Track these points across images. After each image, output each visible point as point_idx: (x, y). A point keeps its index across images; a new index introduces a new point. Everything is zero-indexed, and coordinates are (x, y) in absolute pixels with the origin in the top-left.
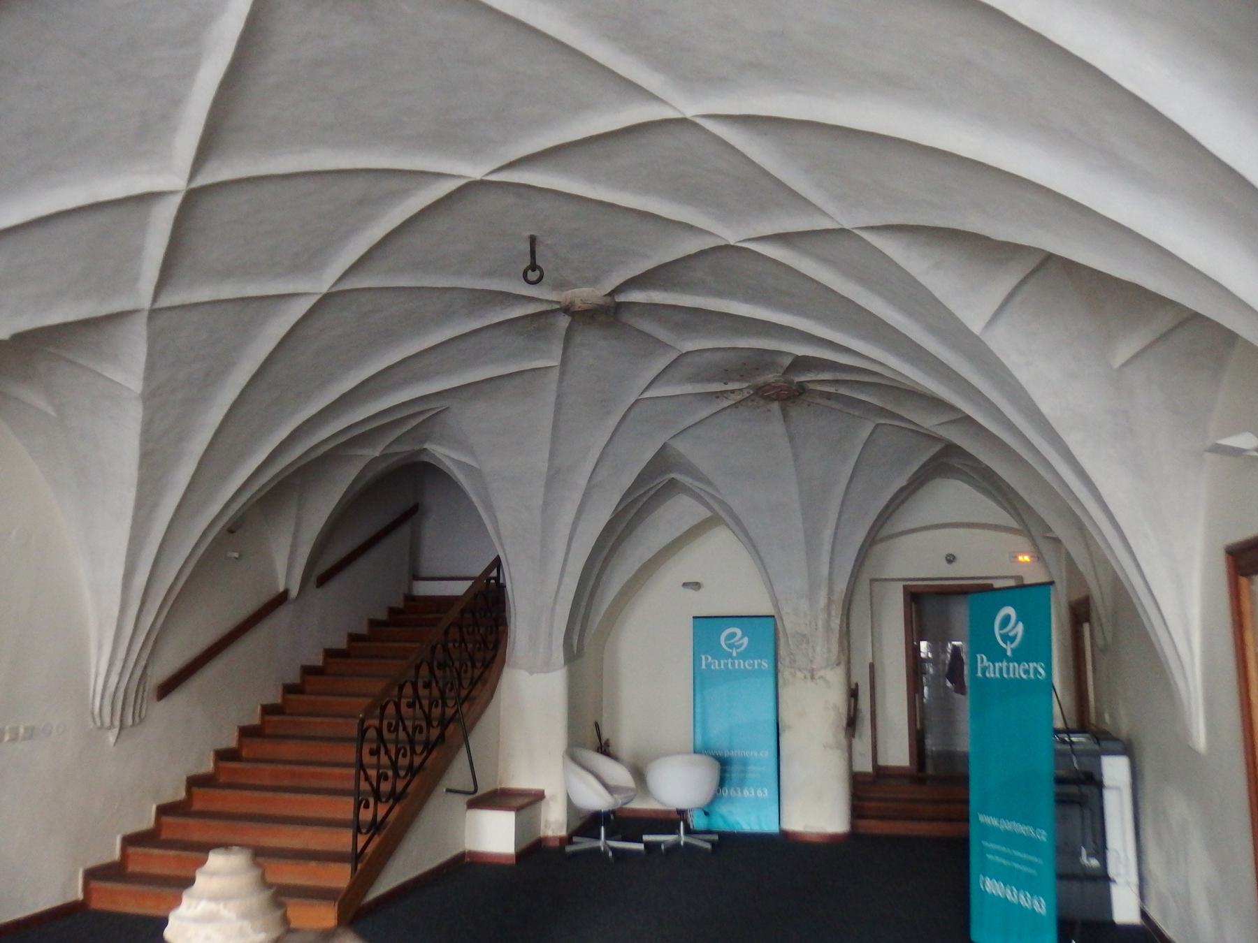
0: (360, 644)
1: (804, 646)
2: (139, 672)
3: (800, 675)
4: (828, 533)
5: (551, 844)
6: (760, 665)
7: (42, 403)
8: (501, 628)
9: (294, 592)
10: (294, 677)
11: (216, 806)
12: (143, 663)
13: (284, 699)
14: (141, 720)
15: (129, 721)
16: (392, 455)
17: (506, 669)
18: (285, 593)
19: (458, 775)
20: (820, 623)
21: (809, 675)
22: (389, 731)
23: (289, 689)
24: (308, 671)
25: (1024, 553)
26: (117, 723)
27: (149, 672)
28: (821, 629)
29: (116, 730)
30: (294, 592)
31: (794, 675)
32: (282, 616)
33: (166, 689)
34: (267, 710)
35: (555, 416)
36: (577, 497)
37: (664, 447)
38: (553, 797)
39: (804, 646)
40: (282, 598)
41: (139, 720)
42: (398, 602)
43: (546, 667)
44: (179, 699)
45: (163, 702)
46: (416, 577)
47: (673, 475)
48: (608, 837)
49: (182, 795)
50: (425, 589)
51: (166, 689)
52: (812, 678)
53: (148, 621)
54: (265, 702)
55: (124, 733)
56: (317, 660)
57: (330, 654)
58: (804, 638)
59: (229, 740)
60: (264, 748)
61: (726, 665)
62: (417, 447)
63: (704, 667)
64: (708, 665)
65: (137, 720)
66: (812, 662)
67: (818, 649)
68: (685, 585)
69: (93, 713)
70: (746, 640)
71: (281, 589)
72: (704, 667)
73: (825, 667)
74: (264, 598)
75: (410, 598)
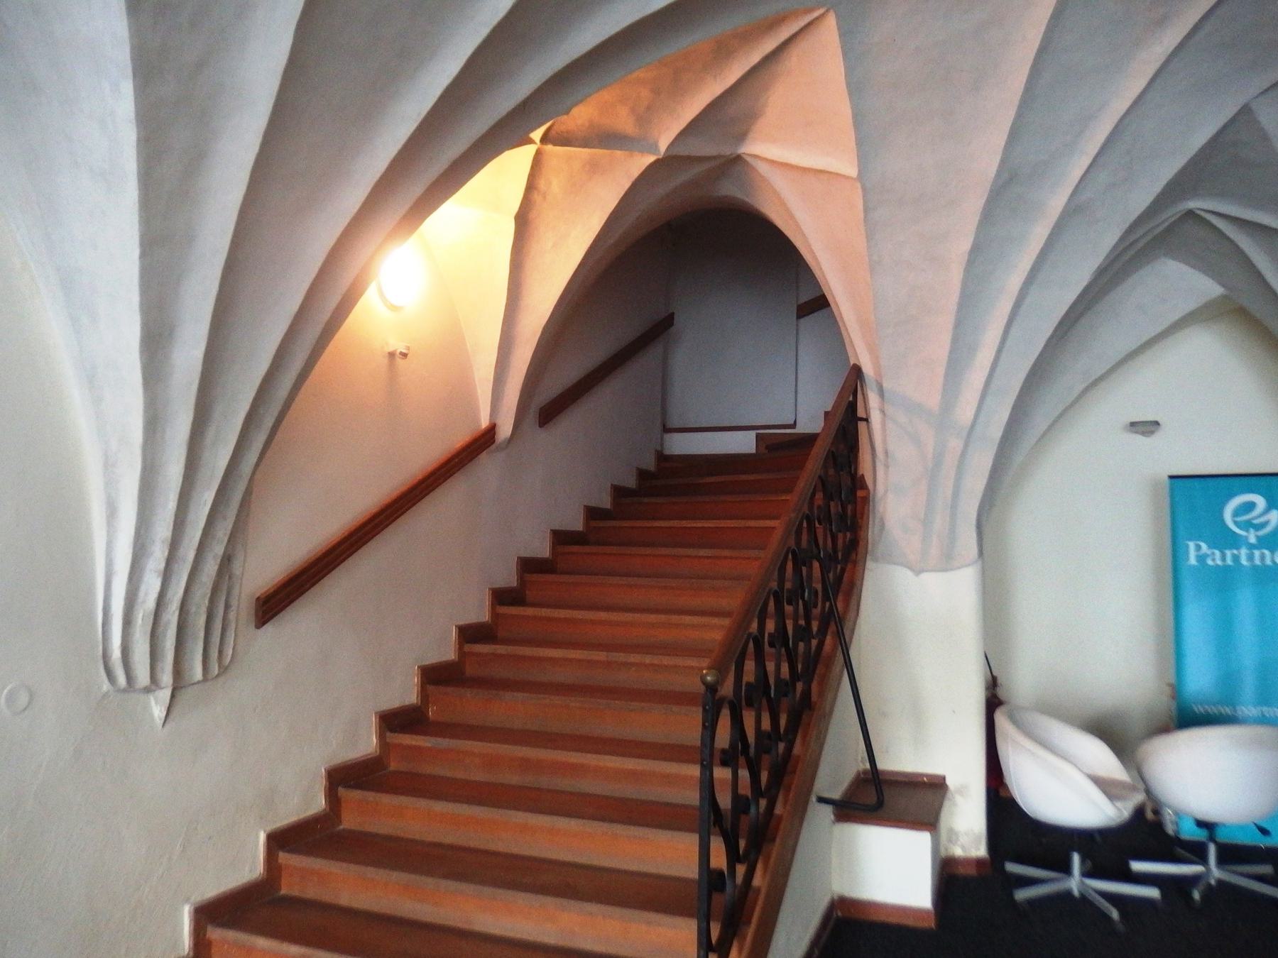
0: (601, 524)
2: (210, 568)
5: (961, 871)
8: (860, 493)
9: (505, 429)
10: (507, 577)
11: (382, 826)
12: (218, 549)
13: (494, 615)
14: (224, 670)
15: (198, 673)
16: (691, 160)
17: (870, 564)
18: (491, 430)
19: (837, 767)
21: (399, 361)
22: (1236, 513)
23: (501, 597)
24: (528, 566)
26: (167, 678)
27: (237, 567)
29: (165, 694)
30: (505, 429)
32: (488, 466)
33: (271, 606)
34: (469, 634)
36: (1039, 233)
38: (962, 790)
40: (485, 440)
41: (220, 665)
42: (650, 463)
43: (947, 562)
44: (303, 620)
45: (269, 628)
46: (667, 430)
47: (1192, 204)
48: (1087, 874)
49: (319, 803)
50: (681, 445)
51: (271, 606)
53: (218, 458)
54: (461, 623)
55: (186, 696)
56: (541, 548)
57: (561, 538)
59: (405, 692)
60: (466, 705)
61: (1236, 558)
62: (727, 151)
63: (1193, 561)
64: (1201, 559)
65: (215, 669)
68: (1133, 424)
69: (106, 657)
71: (484, 423)
72: (1193, 561)
74: (459, 438)
75: (662, 458)
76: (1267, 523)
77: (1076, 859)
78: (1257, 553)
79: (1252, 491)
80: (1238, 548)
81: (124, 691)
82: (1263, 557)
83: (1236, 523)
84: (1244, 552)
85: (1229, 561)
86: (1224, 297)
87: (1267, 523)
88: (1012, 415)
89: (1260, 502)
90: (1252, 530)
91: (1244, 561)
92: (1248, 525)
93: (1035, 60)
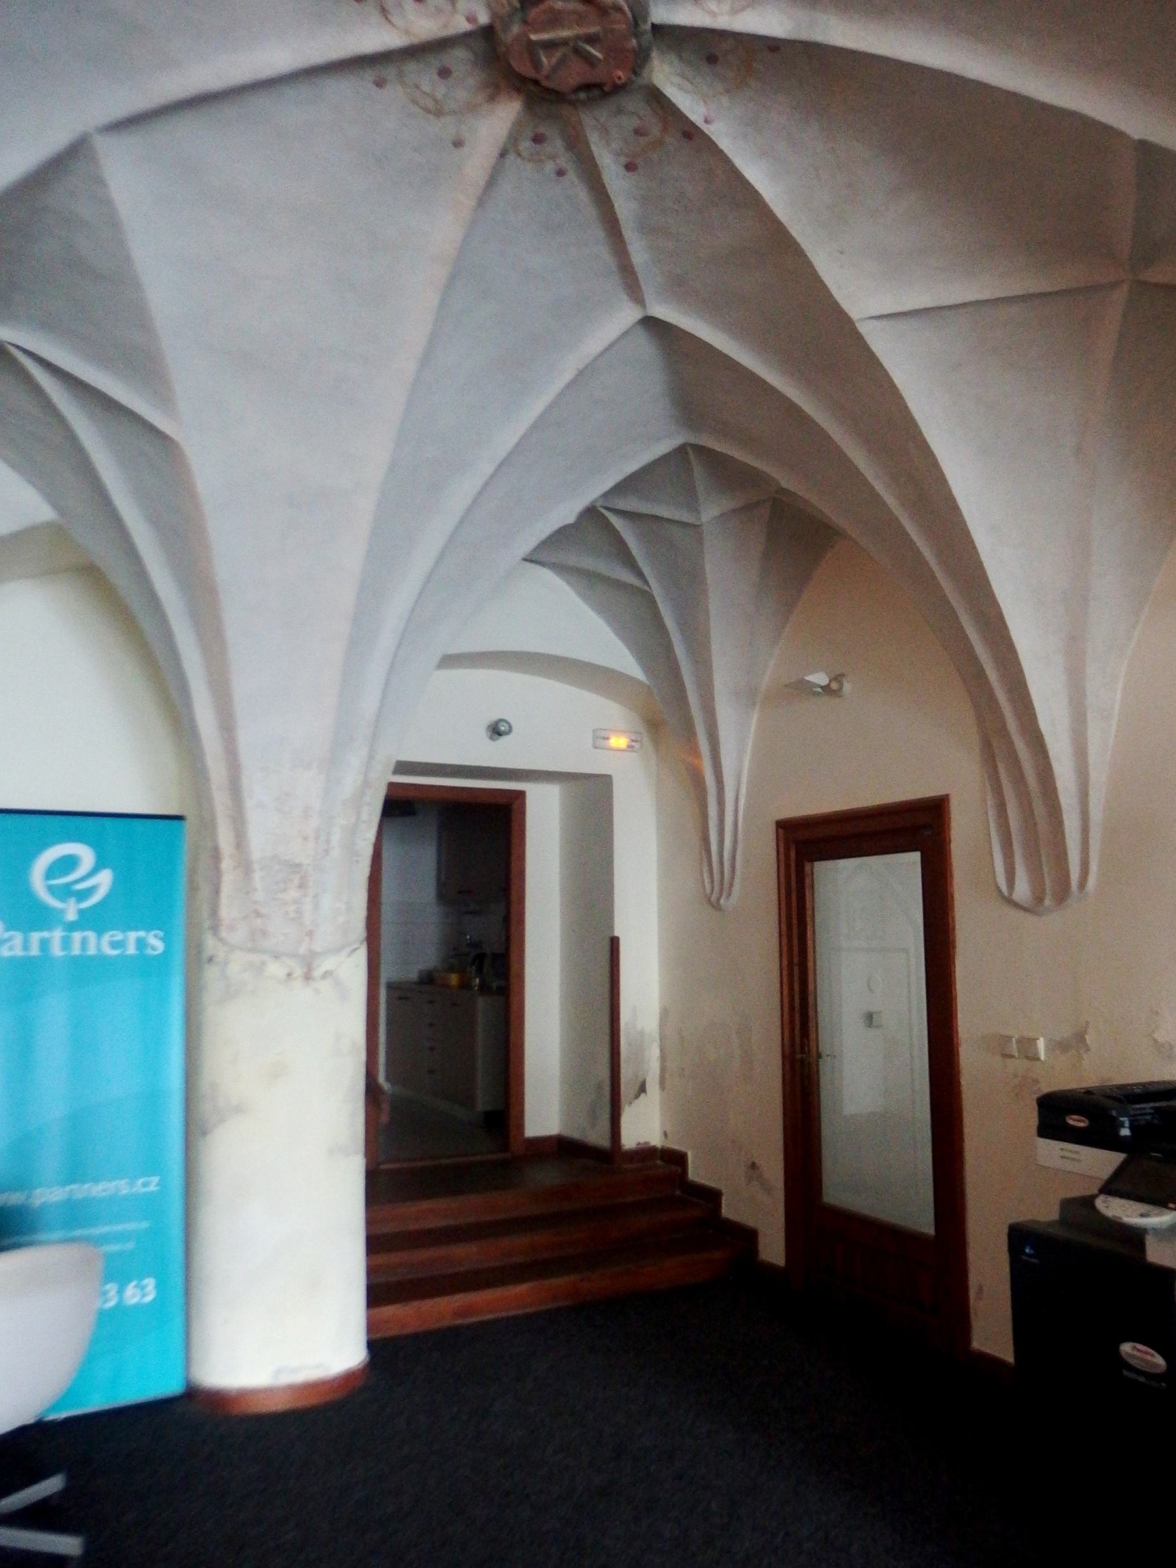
1: (293, 893)
3: (276, 969)
4: (387, 640)
6: (141, 944)
7: (478, 159)
20: (336, 837)
21: (299, 972)
22: (50, 873)
25: (618, 732)
28: (336, 853)
31: (260, 968)
35: (1013, 297)
37: (73, 157)
39: (293, 893)
52: (308, 977)
58: (295, 873)
61: (45, 944)
66: (310, 934)
67: (327, 902)
70: (105, 879)
73: (338, 950)
76: (91, 891)
77: (992, 1331)
78: (77, 936)
79: (79, 840)
80: (49, 928)
81: (292, 919)
82: (84, 943)
83: (50, 889)
84: (57, 934)
85: (35, 951)
86: (49, 525)
87: (91, 891)
88: (518, 444)
89: (86, 855)
90: (72, 900)
91: (57, 951)
92: (65, 893)
93: (522, 653)
